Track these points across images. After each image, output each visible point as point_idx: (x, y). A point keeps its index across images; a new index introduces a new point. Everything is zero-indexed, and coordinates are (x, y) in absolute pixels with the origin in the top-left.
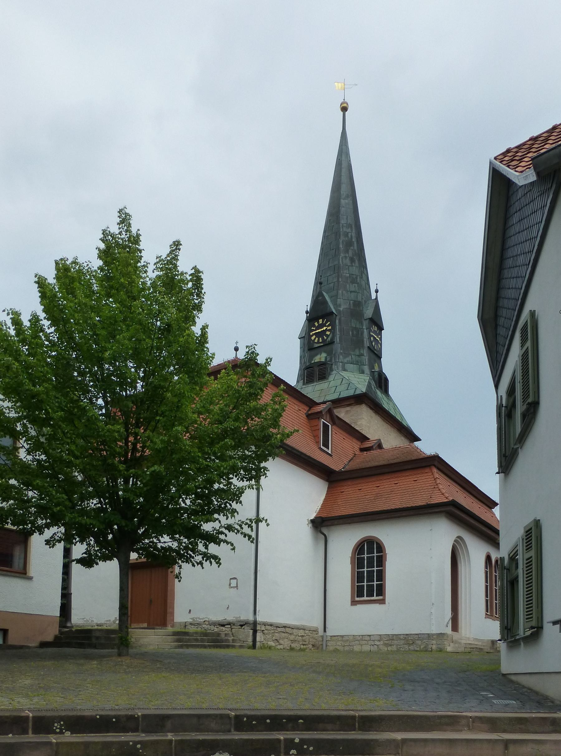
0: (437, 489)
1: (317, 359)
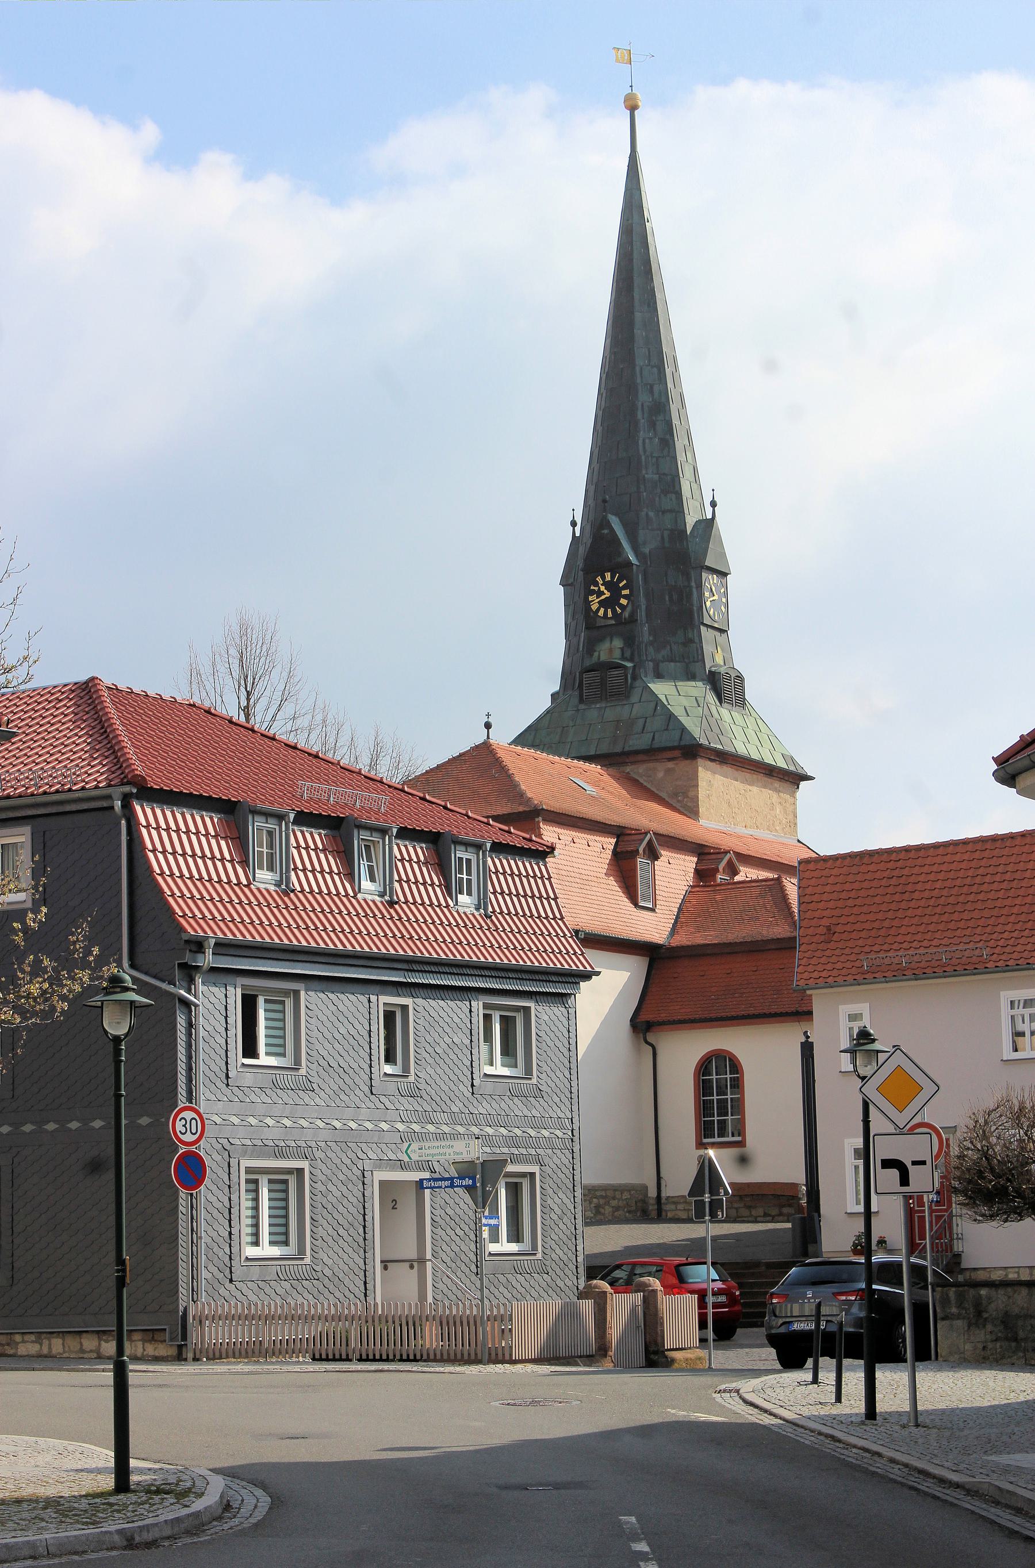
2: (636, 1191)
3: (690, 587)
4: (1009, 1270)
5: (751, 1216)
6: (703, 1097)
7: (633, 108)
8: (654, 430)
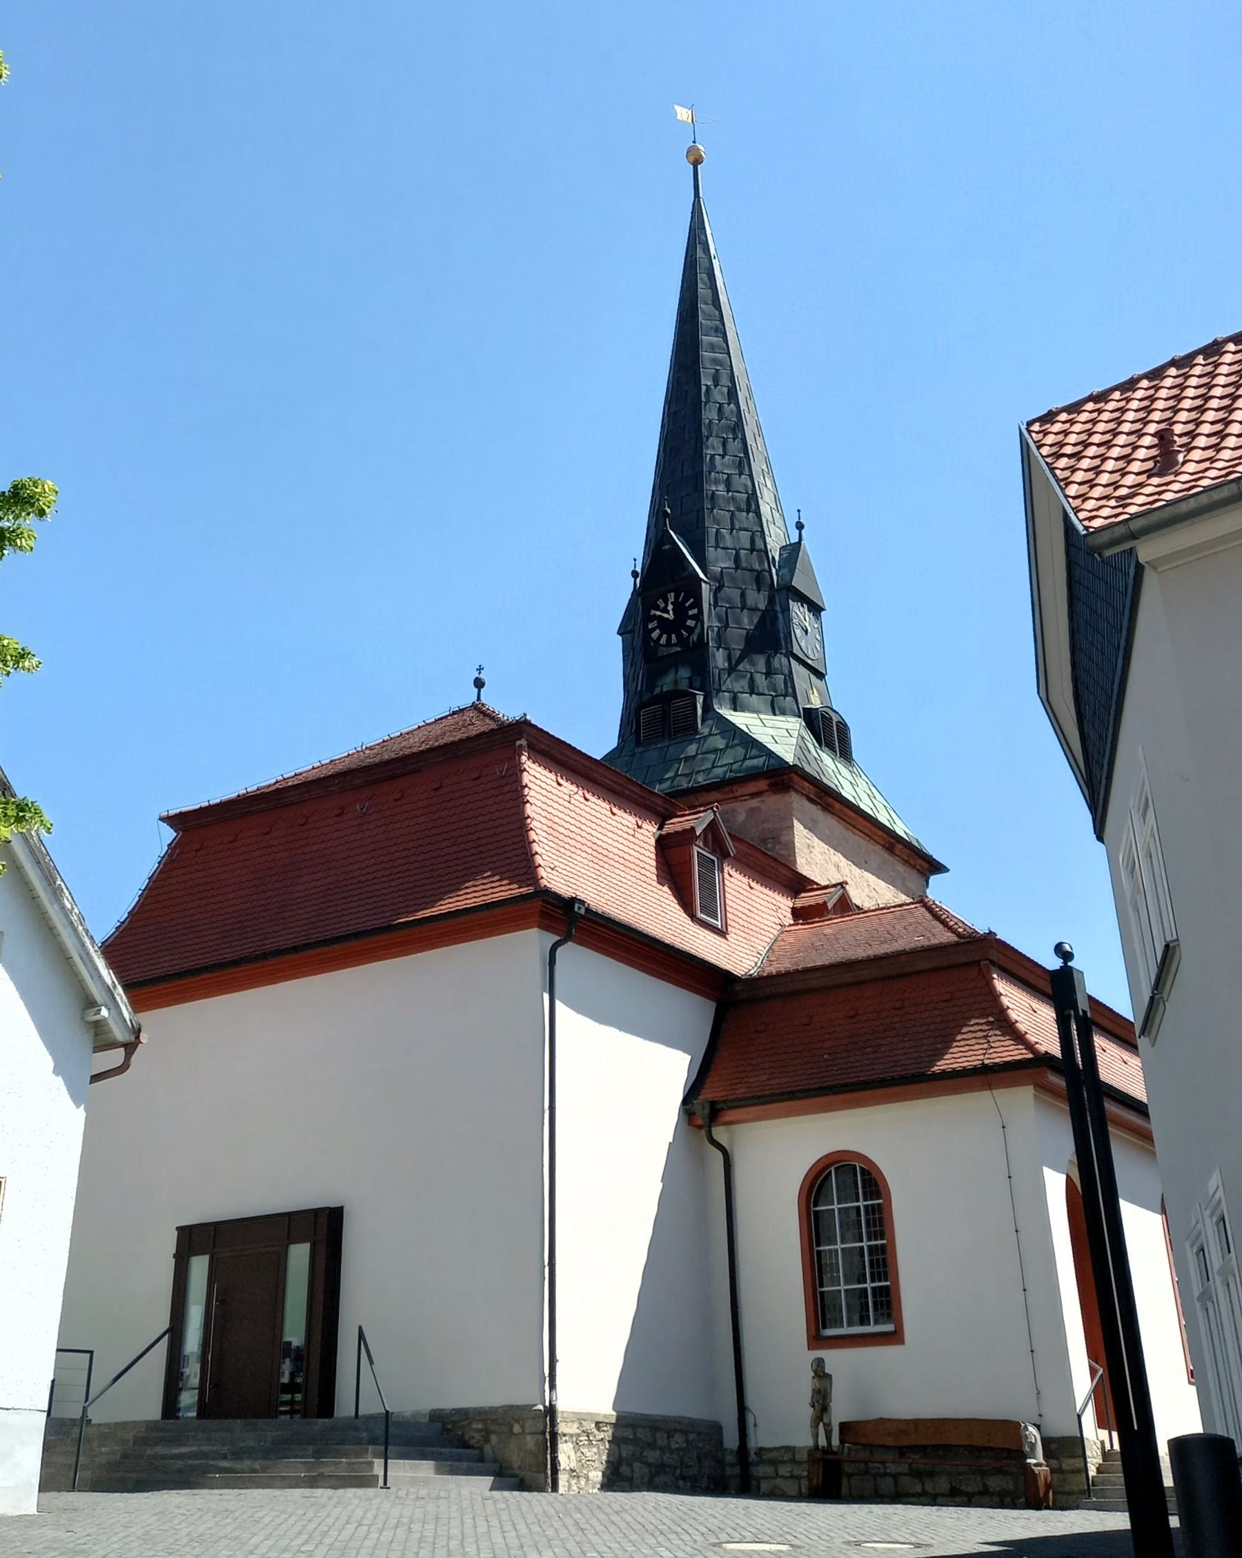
1: (666, 683)
2: (699, 1434)
3: (776, 612)
7: (696, 162)
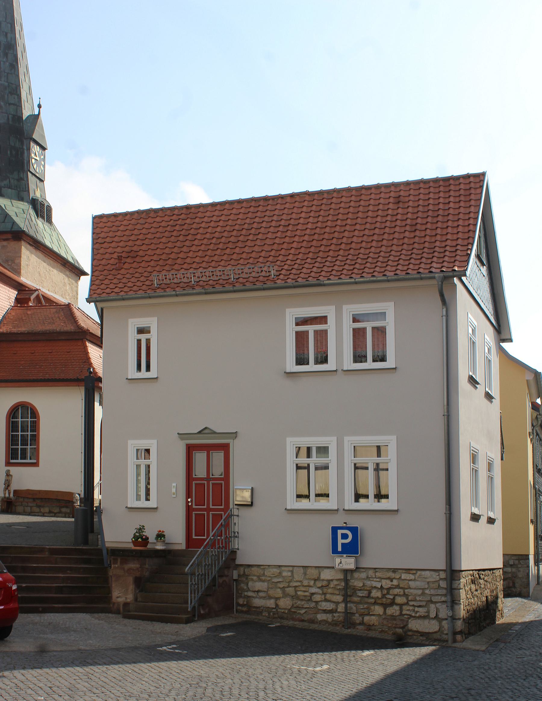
0: (87, 364)
3: (23, 149)
4: (283, 568)
5: (41, 512)
6: (12, 432)
8: (7, 58)
